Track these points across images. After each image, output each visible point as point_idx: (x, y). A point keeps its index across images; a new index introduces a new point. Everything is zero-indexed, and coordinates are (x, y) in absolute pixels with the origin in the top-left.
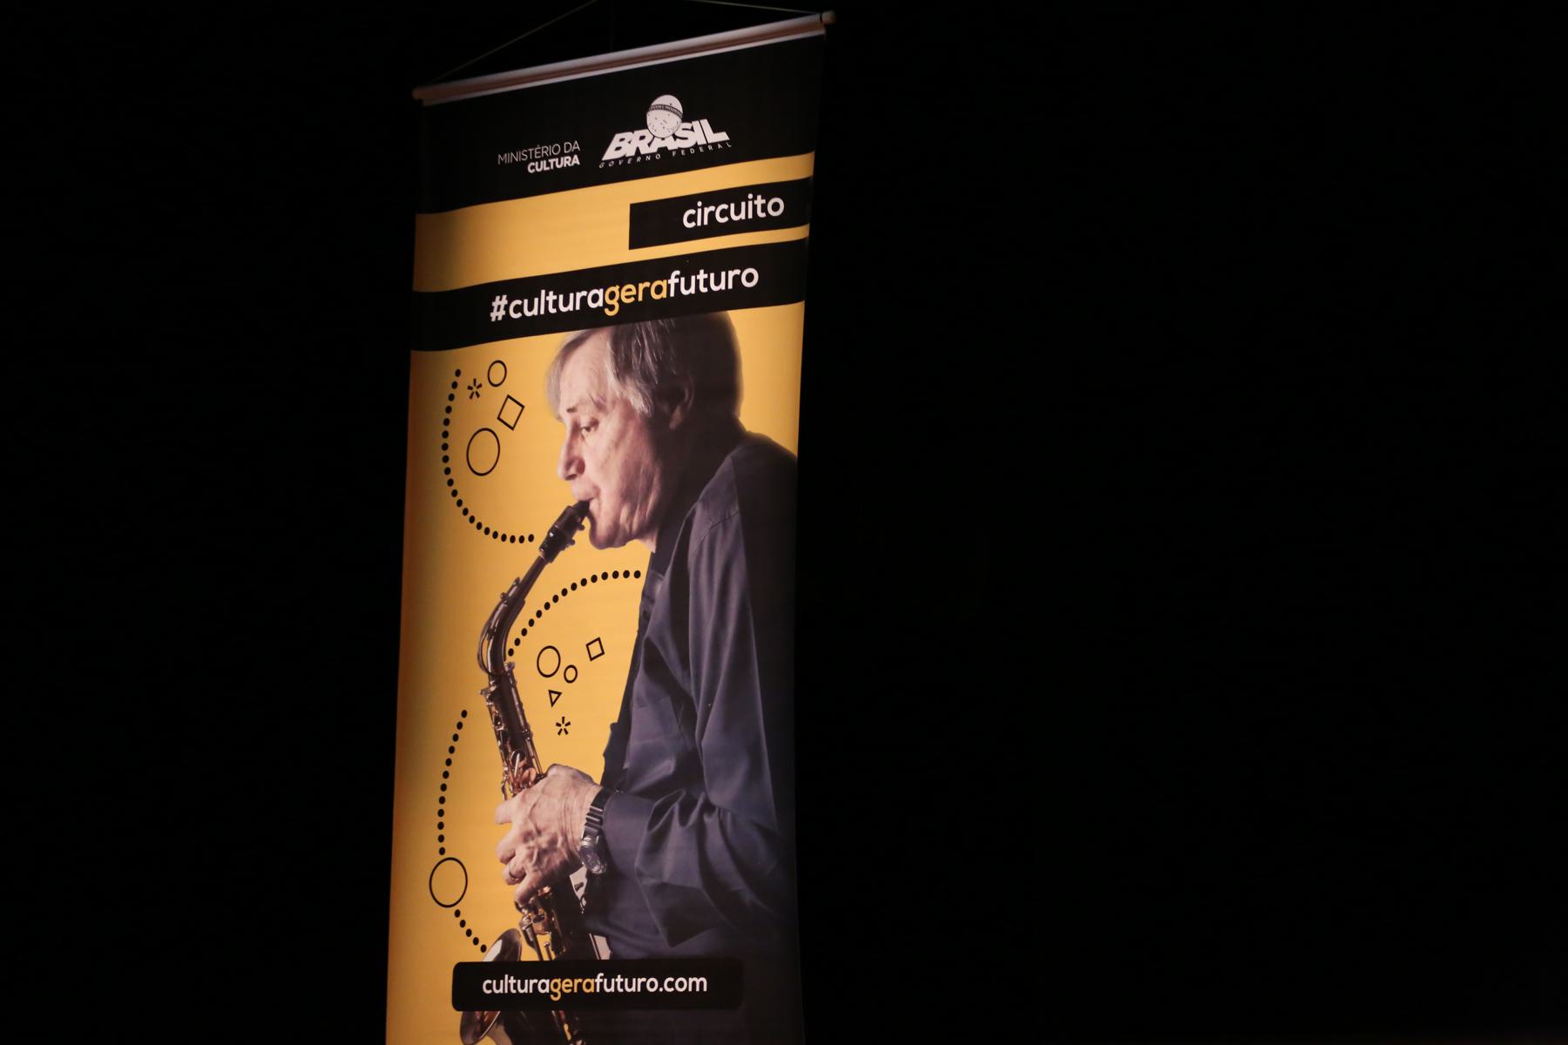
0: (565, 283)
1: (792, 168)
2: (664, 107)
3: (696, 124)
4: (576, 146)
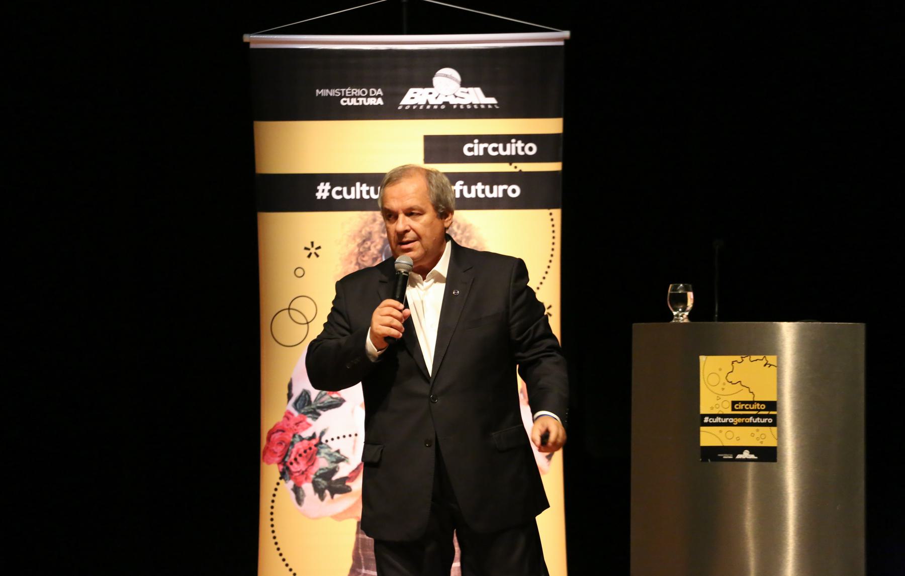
1: (553, 126)
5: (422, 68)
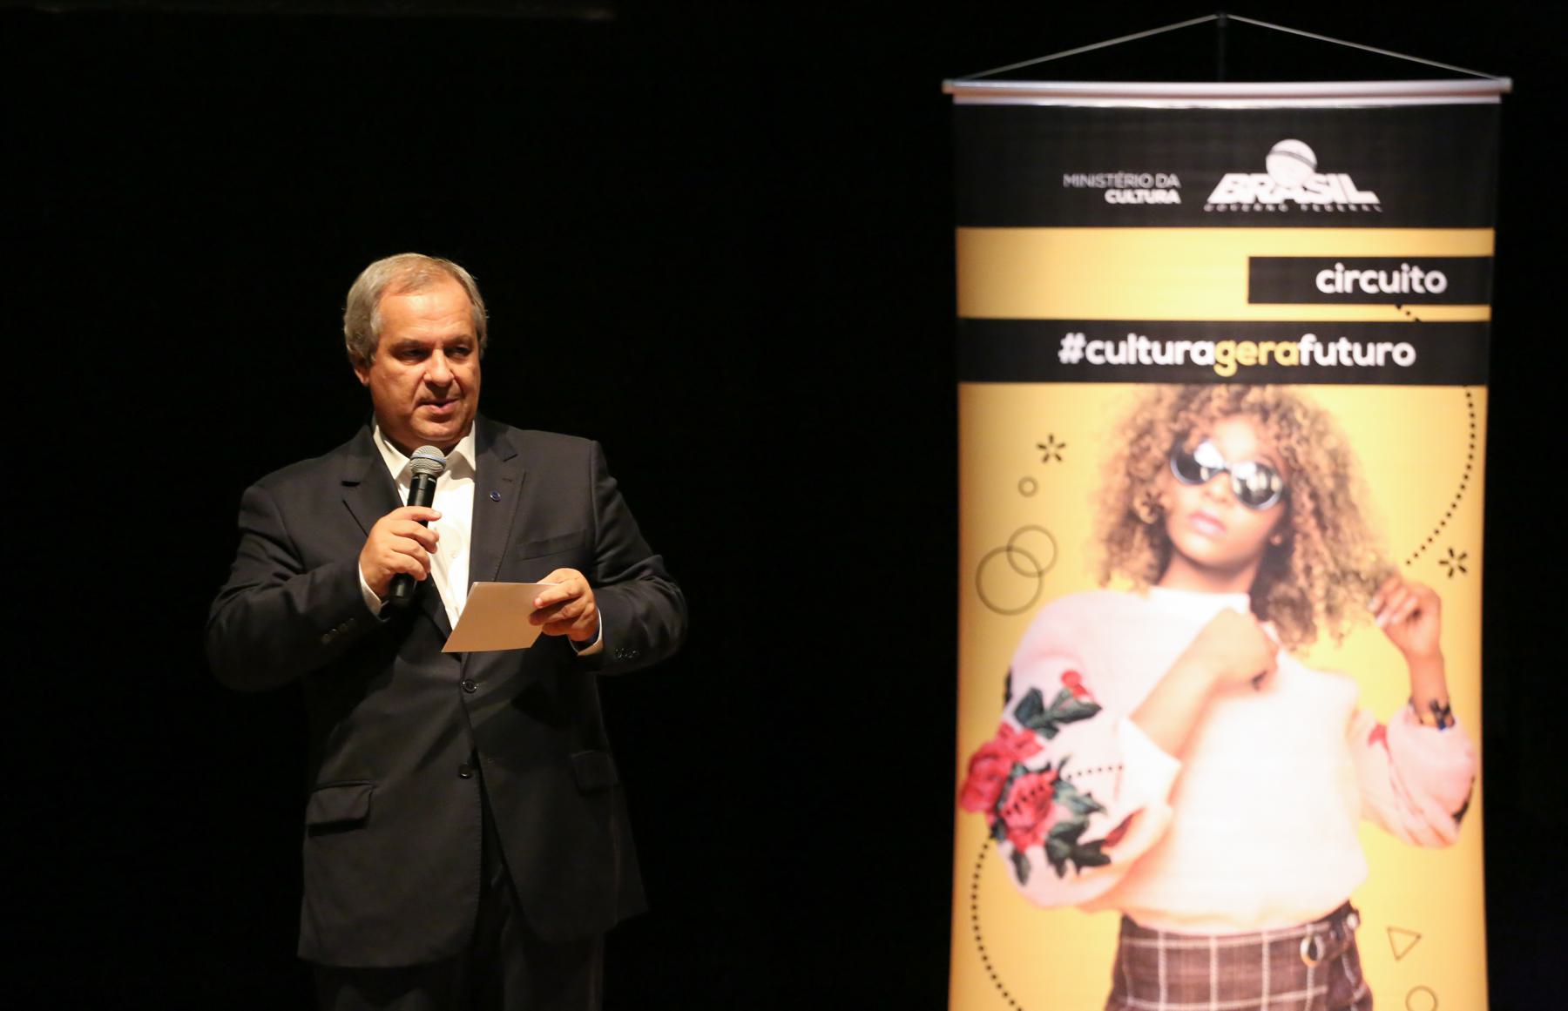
0: (1162, 331)
1: (1475, 243)
2: (1291, 154)
3: (1332, 178)
4: (1173, 180)
5: (1248, 141)
